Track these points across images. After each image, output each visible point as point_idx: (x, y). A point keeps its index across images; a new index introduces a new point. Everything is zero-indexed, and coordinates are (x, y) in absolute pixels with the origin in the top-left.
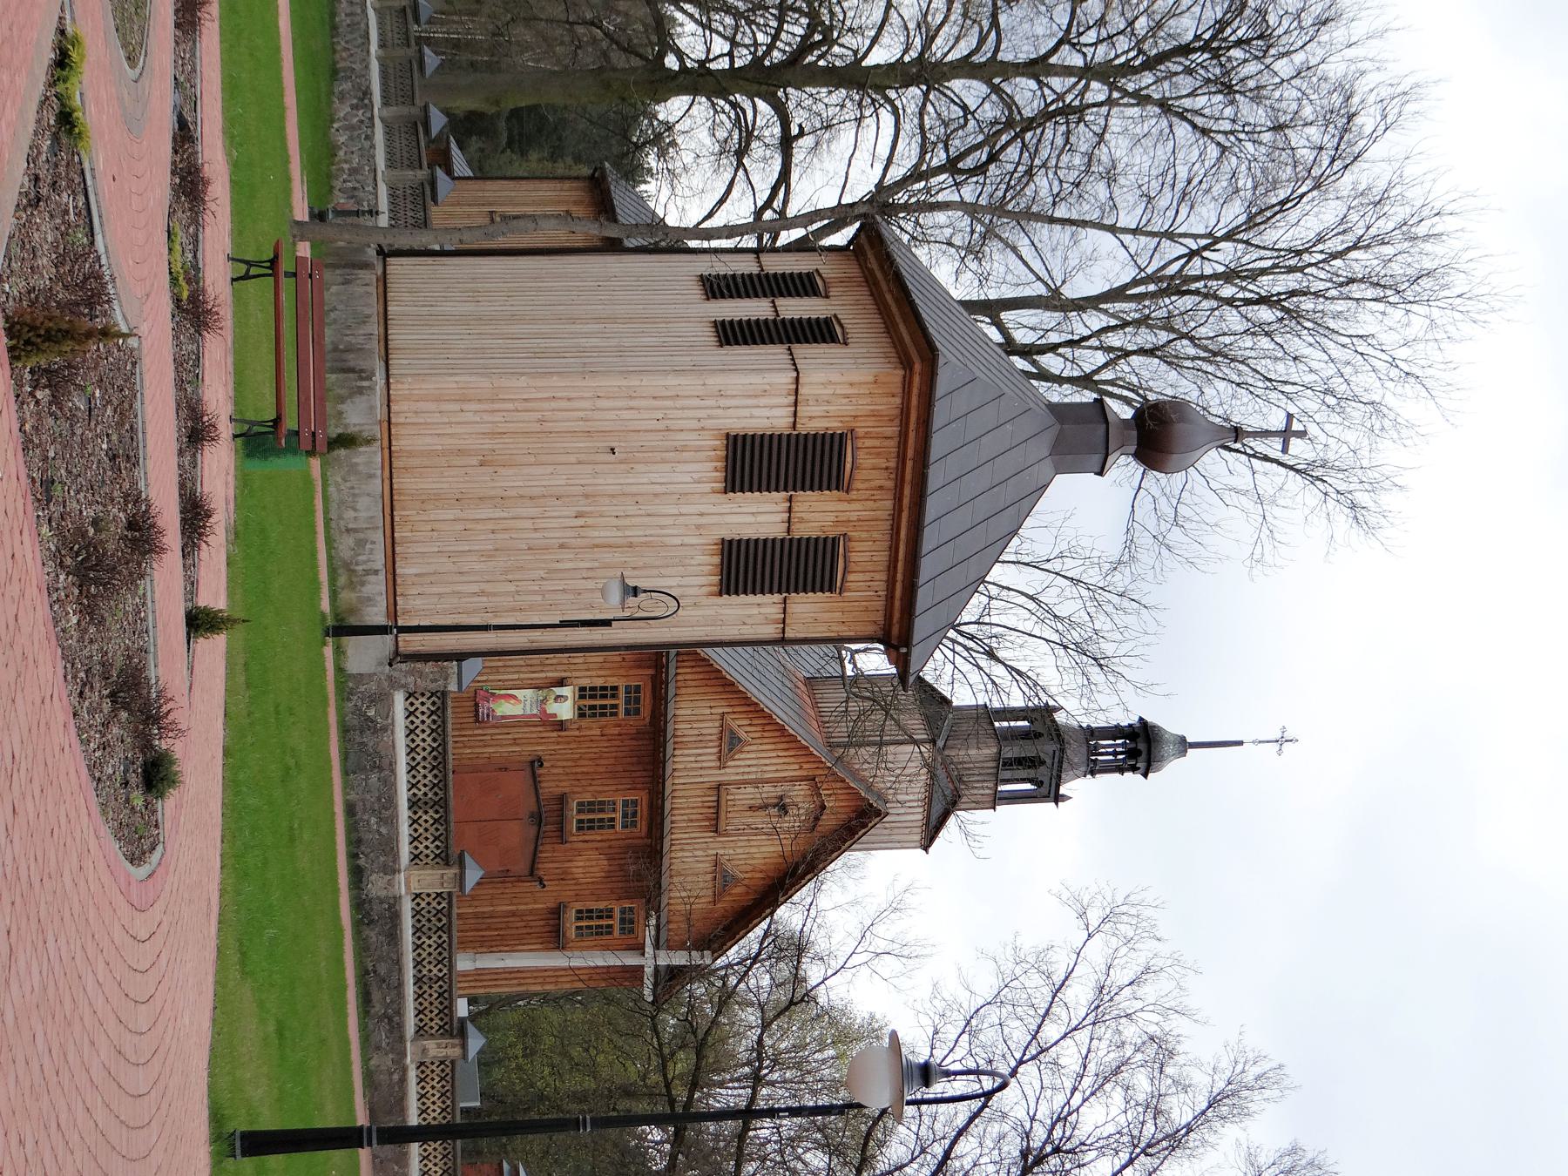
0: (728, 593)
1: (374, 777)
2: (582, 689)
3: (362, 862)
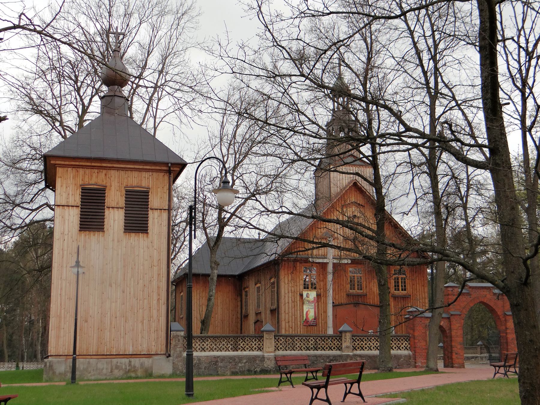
0: (147, 230)
1: (220, 364)
2: (305, 288)
3: (258, 370)
